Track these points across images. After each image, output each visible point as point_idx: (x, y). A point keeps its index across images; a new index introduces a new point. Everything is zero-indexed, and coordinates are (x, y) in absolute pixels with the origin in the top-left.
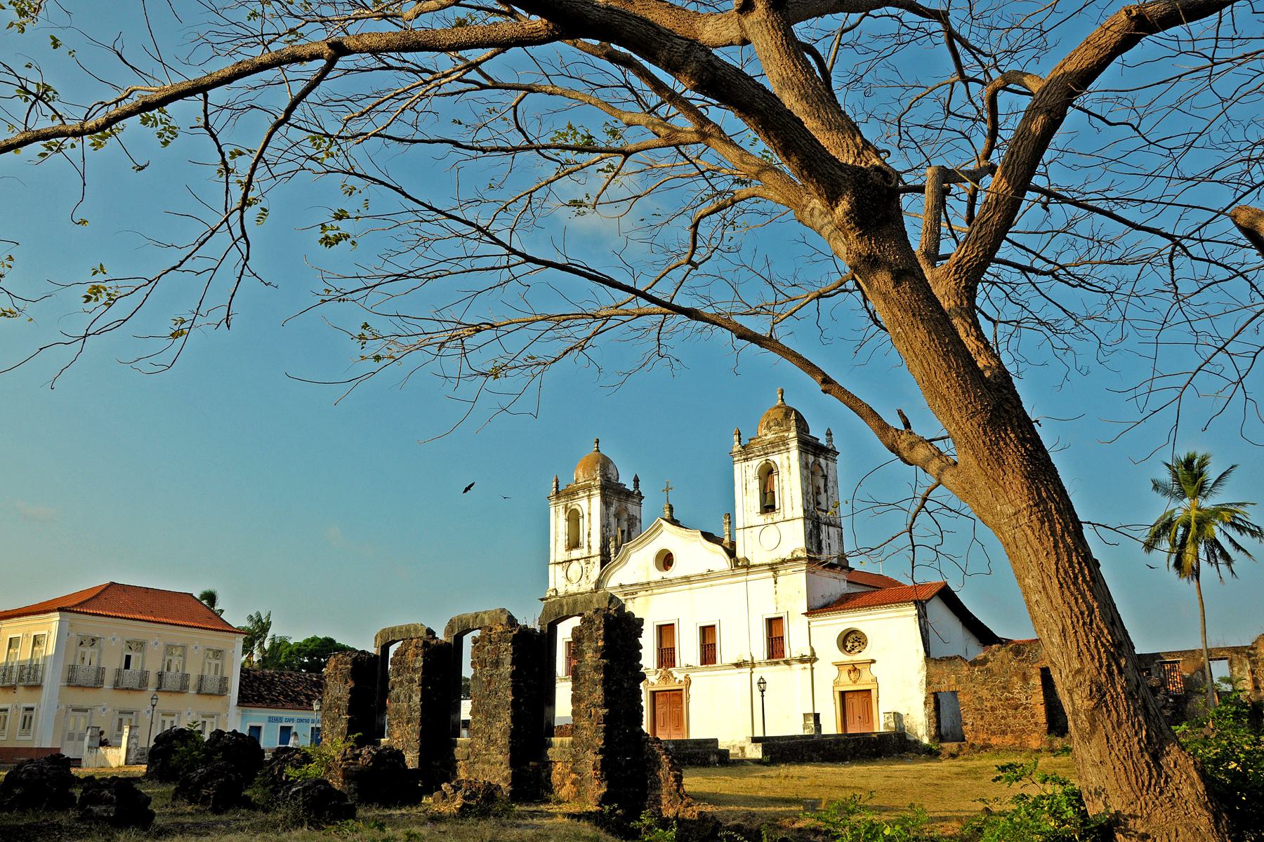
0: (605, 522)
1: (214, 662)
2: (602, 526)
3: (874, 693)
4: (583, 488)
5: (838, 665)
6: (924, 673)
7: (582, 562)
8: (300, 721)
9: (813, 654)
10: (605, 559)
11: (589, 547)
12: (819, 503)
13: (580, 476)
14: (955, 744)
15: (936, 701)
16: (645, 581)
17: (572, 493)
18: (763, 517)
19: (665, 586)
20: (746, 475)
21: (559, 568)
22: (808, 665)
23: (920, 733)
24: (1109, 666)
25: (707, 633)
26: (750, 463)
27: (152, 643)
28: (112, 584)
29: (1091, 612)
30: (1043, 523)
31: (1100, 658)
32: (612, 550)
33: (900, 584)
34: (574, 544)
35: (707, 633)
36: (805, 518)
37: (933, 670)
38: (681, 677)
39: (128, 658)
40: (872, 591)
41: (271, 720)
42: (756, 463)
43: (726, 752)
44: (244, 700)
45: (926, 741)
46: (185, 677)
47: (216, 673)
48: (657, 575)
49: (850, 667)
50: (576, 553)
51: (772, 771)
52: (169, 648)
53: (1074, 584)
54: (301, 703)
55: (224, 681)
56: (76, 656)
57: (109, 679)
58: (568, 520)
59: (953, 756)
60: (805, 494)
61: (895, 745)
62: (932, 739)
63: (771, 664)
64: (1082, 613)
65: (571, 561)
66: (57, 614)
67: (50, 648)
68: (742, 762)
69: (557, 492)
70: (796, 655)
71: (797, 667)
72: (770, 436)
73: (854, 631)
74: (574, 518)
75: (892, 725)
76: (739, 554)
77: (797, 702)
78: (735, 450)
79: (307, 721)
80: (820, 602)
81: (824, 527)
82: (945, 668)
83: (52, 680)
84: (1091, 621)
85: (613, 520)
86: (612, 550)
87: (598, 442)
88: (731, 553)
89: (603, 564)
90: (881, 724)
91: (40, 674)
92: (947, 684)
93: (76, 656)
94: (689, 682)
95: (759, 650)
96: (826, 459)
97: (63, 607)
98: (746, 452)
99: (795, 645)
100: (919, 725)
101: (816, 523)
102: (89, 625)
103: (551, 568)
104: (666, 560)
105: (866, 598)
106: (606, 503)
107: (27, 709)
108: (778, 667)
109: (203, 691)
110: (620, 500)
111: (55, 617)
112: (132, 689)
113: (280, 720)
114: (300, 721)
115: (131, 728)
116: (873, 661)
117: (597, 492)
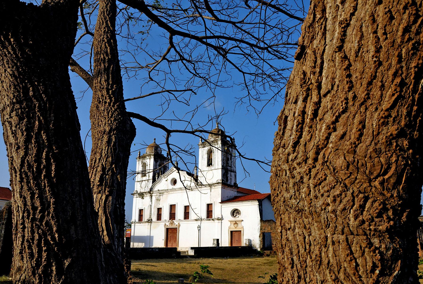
0: (155, 168)
3: (242, 232)
4: (148, 155)
5: (231, 221)
6: (260, 225)
7: (146, 181)
9: (222, 217)
10: (154, 180)
12: (228, 164)
13: (148, 151)
14: (269, 251)
15: (264, 236)
16: (166, 189)
17: (144, 157)
18: (208, 168)
20: (203, 152)
21: (138, 183)
22: (220, 221)
23: (257, 247)
24: (49, 265)
26: (205, 148)
29: (45, 206)
30: (21, 119)
31: (40, 256)
32: (157, 178)
33: (259, 193)
35: (186, 208)
36: (222, 169)
37: (263, 224)
38: (177, 223)
40: (244, 195)
42: (207, 148)
43: (180, 252)
45: (259, 250)
48: (171, 187)
49: (235, 222)
51: (198, 261)
53: (35, 179)
58: (143, 166)
59: (268, 256)
60: (223, 160)
61: (248, 251)
62: (261, 249)
64: (34, 208)
68: (186, 257)
69: (140, 156)
70: (216, 217)
71: (216, 221)
72: (212, 139)
73: (237, 210)
75: (248, 244)
77: (215, 234)
78: (200, 143)
80: (225, 199)
81: (229, 172)
82: (267, 224)
84: (42, 218)
86: (157, 178)
87: (155, 139)
88: (196, 180)
89: (153, 182)
90: (244, 243)
92: (268, 229)
94: (179, 226)
95: (204, 215)
96: (232, 148)
99: (216, 214)
100: (257, 244)
101: (227, 169)
103: (136, 183)
105: (242, 198)
106: (156, 160)
108: (210, 221)
110: (161, 160)
116: (242, 221)
117: (152, 157)
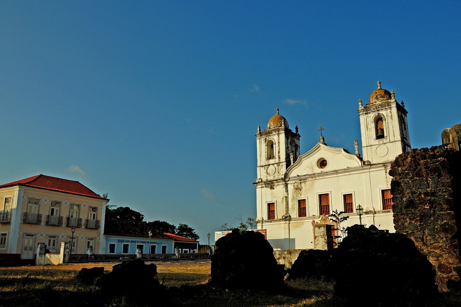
1: (93, 213)
2: (286, 148)
4: (275, 130)
8: (132, 242)
10: (288, 164)
11: (279, 158)
17: (269, 133)
18: (377, 141)
19: (349, 172)
20: (366, 122)
21: (262, 169)
25: (347, 198)
26: (369, 115)
27: (64, 203)
28: (41, 175)
32: (292, 159)
34: (270, 156)
39: (53, 210)
41: (120, 241)
44: (107, 232)
46: (80, 220)
47: (94, 218)
48: (318, 170)
50: (272, 161)
52: (72, 205)
54: (131, 233)
55: (98, 222)
56: (27, 208)
57: (44, 219)
58: (267, 145)
63: (385, 212)
65: (270, 165)
66: (18, 186)
67: (14, 205)
69: (260, 133)
72: (378, 102)
74: (271, 145)
76: (365, 159)
79: (135, 242)
83: (15, 220)
85: (289, 145)
86: (292, 159)
87: (278, 110)
89: (287, 166)
91: (9, 217)
93: (27, 208)
97: (19, 184)
98: (367, 110)
102: (35, 193)
103: (258, 169)
104: (322, 163)
107: (3, 235)
109: (88, 227)
111: (17, 188)
112: (55, 225)
113: (123, 241)
114: (132, 242)
115: (65, 243)
